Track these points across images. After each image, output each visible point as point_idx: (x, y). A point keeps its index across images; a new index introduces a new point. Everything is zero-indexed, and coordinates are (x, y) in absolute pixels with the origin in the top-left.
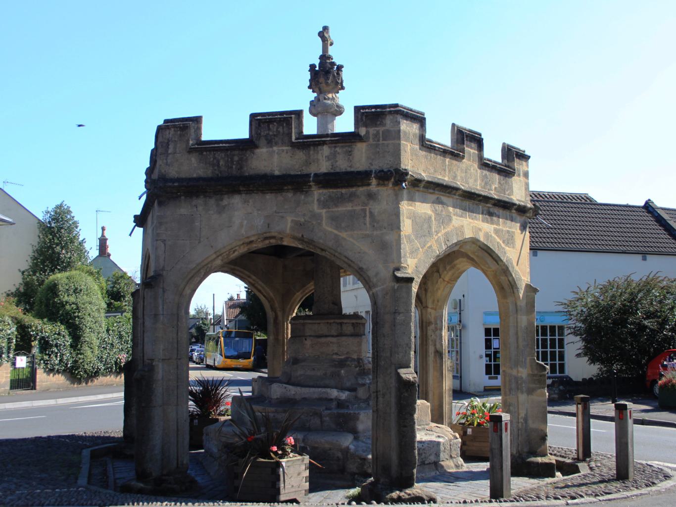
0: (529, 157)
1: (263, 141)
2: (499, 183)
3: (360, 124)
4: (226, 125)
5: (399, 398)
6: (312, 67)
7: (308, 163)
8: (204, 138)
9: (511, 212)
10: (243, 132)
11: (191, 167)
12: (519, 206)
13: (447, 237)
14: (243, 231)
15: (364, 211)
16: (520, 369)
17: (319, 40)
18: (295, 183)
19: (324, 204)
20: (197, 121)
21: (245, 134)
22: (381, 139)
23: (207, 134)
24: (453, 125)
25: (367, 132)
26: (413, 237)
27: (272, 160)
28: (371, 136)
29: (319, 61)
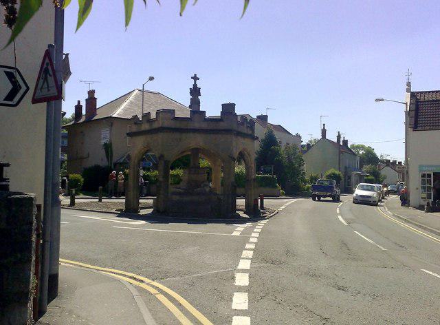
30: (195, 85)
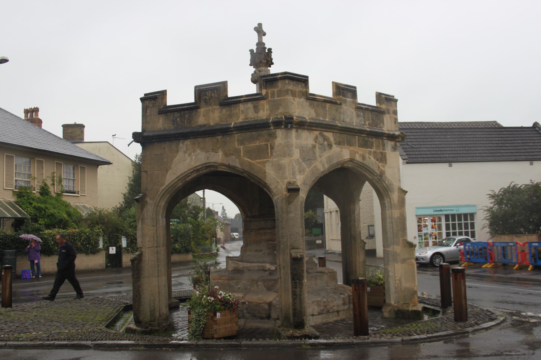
0: (166, 91)
1: (203, 103)
2: (372, 119)
3: (263, 87)
4: (180, 95)
5: (293, 269)
6: (251, 51)
7: (231, 116)
8: (169, 104)
9: (382, 139)
10: (191, 99)
11: (161, 124)
12: (389, 134)
13: (329, 159)
14: (193, 163)
15: (267, 145)
16: (395, 247)
17: (256, 34)
18: (222, 131)
19: (241, 143)
20: (163, 93)
21: (192, 100)
22: (276, 96)
23: (170, 101)
24: (333, 82)
25: (267, 93)
26: (300, 160)
27: (210, 116)
28: (269, 95)
29: (256, 47)
30: (261, 45)
